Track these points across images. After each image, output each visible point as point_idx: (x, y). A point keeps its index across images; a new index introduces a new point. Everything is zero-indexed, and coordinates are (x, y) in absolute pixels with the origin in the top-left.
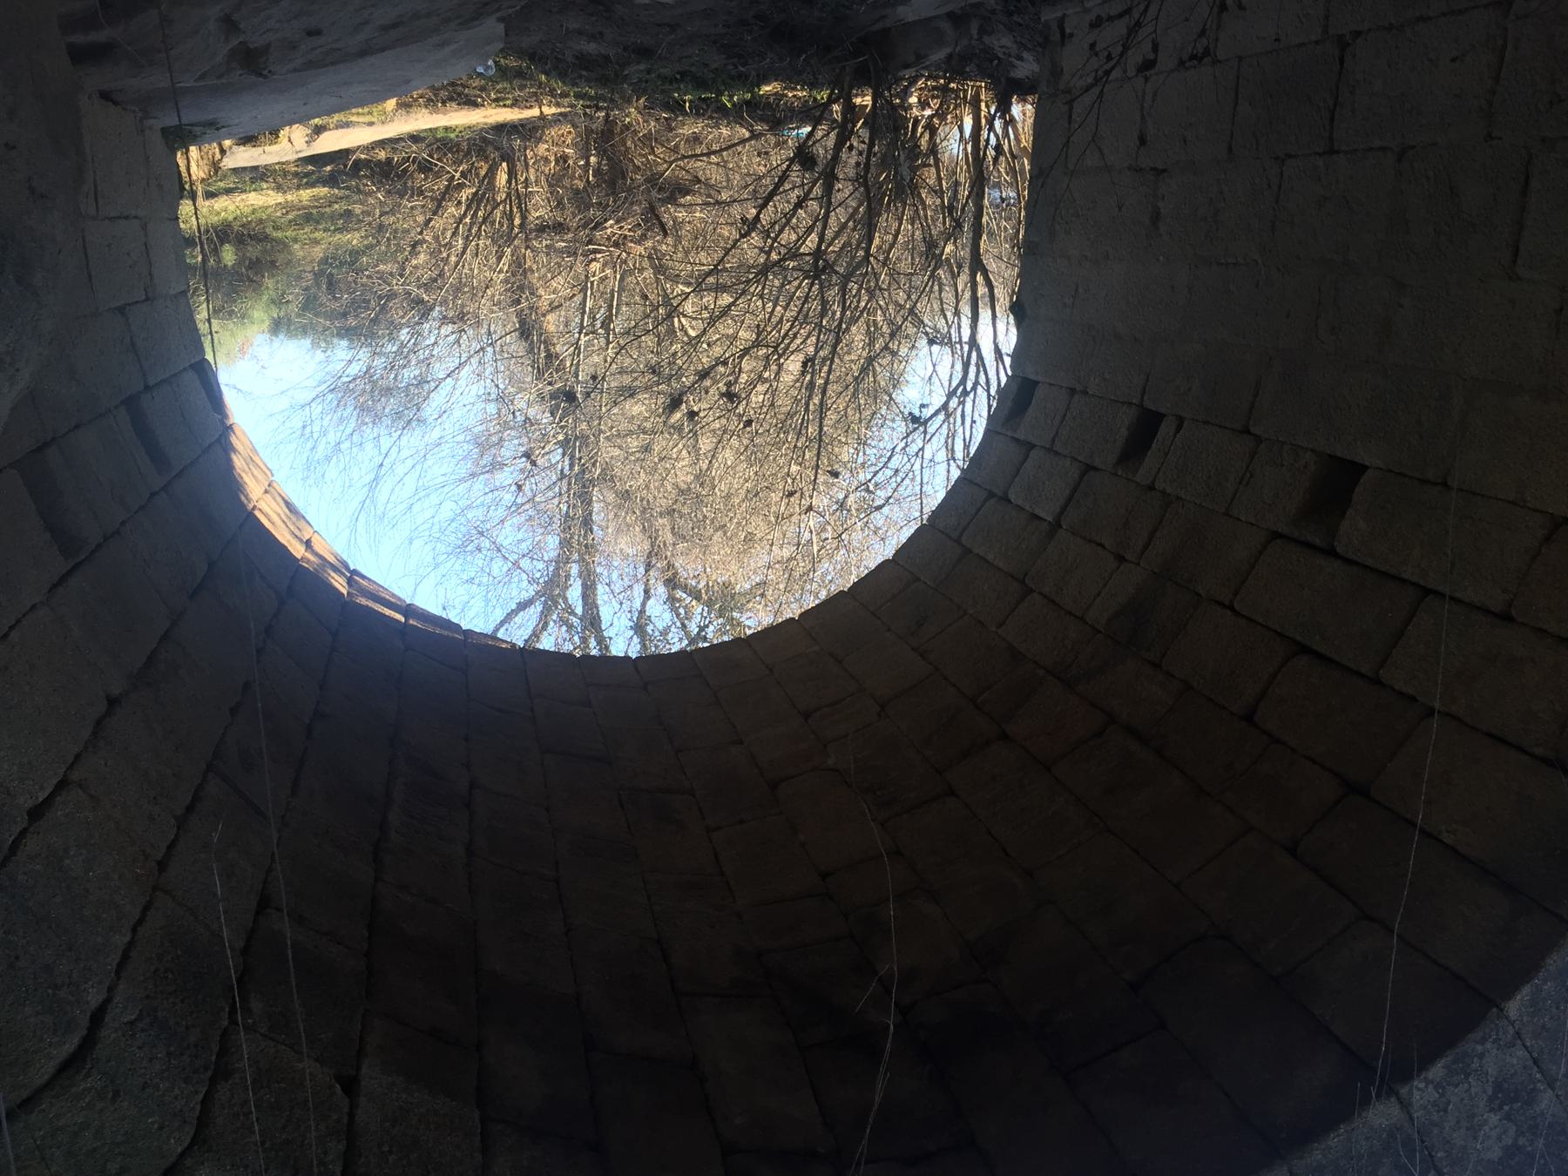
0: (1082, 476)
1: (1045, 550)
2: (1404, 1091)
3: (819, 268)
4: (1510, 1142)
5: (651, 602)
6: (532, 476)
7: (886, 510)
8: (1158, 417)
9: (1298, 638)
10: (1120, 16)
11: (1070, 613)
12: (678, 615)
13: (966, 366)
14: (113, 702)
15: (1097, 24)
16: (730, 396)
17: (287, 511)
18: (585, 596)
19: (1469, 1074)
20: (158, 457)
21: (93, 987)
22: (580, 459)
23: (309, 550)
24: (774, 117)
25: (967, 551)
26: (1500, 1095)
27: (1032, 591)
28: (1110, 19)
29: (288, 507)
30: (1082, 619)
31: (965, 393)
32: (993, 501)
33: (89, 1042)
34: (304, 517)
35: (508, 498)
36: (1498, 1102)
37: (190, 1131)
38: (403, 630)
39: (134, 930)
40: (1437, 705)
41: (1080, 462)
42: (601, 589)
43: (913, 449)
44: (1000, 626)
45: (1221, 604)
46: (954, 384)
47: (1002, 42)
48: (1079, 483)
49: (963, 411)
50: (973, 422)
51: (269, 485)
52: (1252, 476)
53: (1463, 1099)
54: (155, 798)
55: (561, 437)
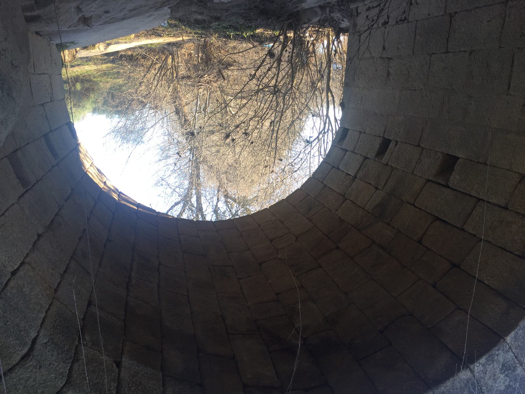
0: (364, 160)
2: (472, 367)
3: (276, 91)
4: (507, 384)
5: (219, 203)
6: (180, 160)
7: (298, 172)
8: (390, 141)
9: (436, 215)
10: (376, 6)
13: (325, 124)
15: (369, 9)
17: (98, 172)
20: (55, 154)
21: (32, 331)
22: (196, 155)
23: (105, 185)
24: (261, 40)
25: (325, 186)
26: (504, 368)
28: (373, 7)
29: (98, 171)
30: (364, 209)
31: (325, 133)
32: (334, 169)
33: (31, 350)
34: (104, 174)
35: (172, 168)
36: (503, 371)
39: (46, 312)
40: (483, 237)
41: (363, 156)
42: (203, 198)
43: (307, 152)
45: (410, 204)
46: (321, 130)
47: (337, 15)
50: (327, 142)
51: (92, 164)
52: (421, 161)
53: (492, 370)
54: (53, 268)
55: (189, 148)
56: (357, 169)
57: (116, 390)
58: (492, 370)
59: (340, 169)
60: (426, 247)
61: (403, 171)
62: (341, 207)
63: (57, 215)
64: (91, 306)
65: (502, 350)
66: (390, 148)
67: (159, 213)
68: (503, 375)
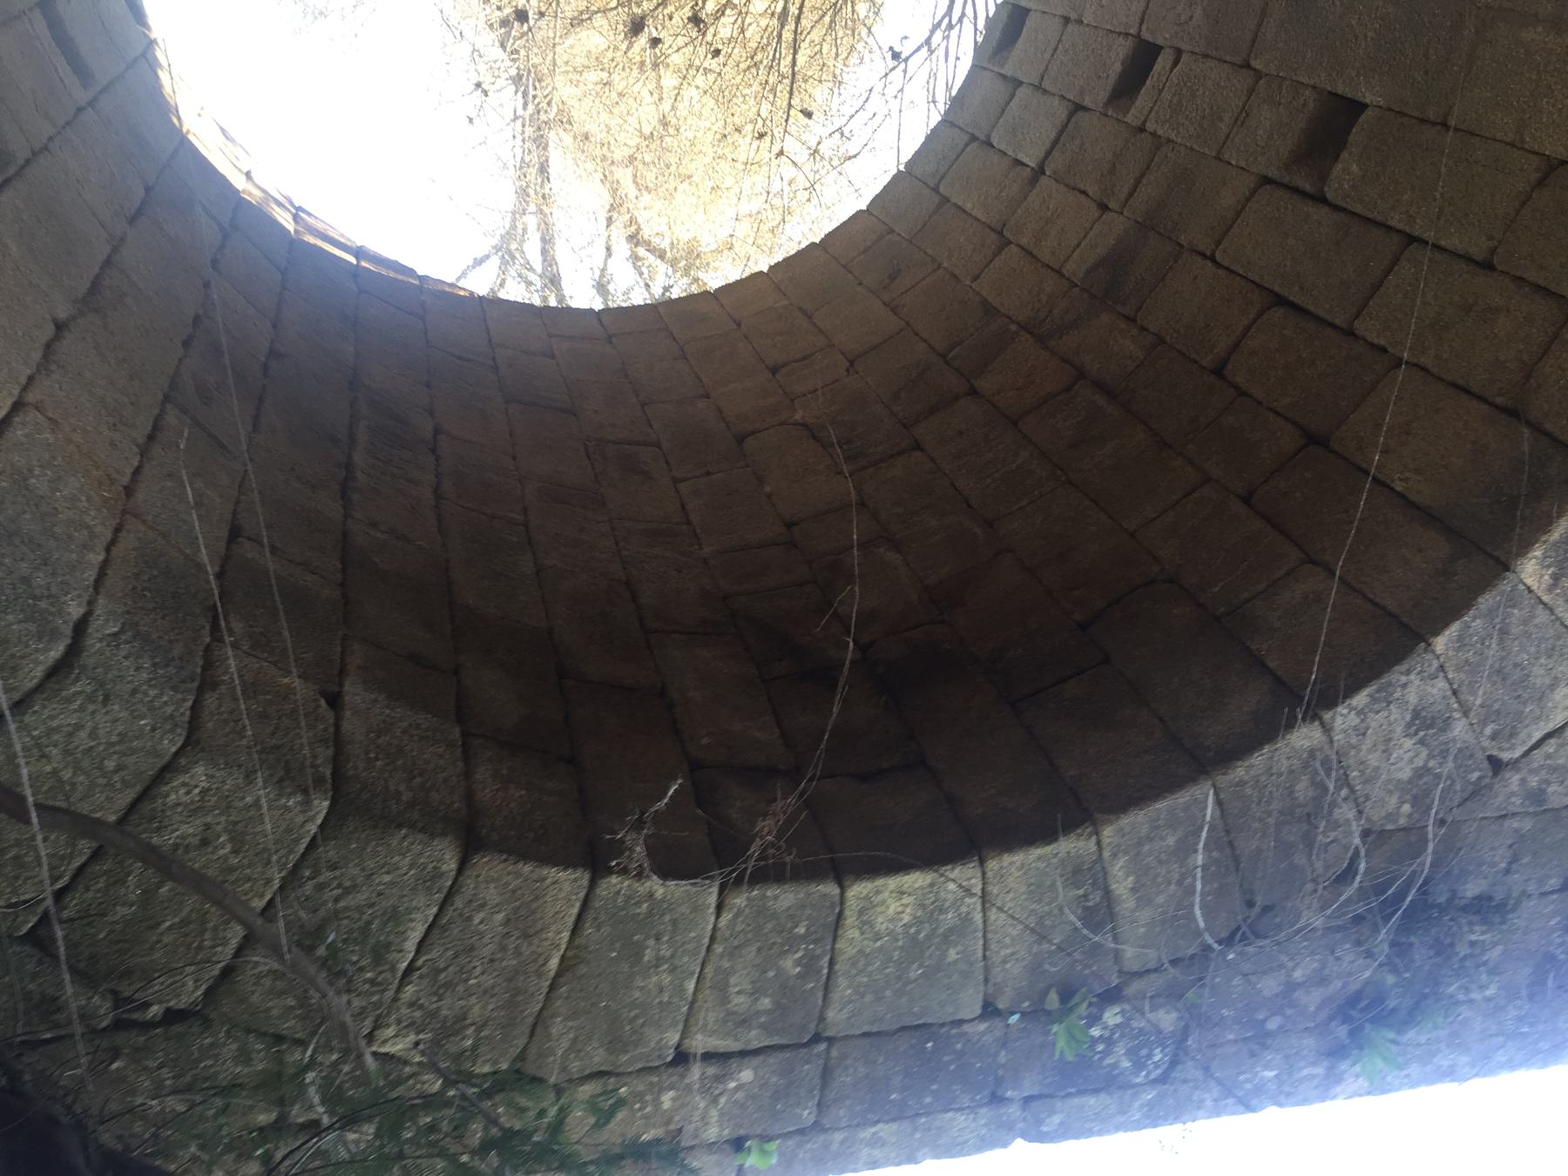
0: (1071, 115)
1: (1026, 198)
4: (1421, 763)
9: (1277, 289)
11: (1048, 266)
12: (641, 274)
14: (60, 327)
16: (695, 20)
18: (544, 252)
19: (1391, 702)
21: (72, 600)
22: (534, 97)
23: (250, 182)
26: (1417, 722)
27: (1010, 243)
30: (1058, 272)
31: (950, 27)
32: (975, 145)
33: (74, 650)
37: (181, 733)
38: (356, 272)
39: (108, 549)
41: (1069, 100)
43: (891, 91)
44: (975, 278)
48: (1067, 124)
49: (947, 48)
50: (958, 58)
52: (1247, 115)
54: (114, 425)
55: (513, 72)
56: (1048, 145)
57: (331, 766)
58: (1384, 727)
59: (993, 147)
60: (1236, 387)
61: (1192, 149)
62: (991, 266)
63: (108, 263)
64: (241, 539)
65: (1418, 674)
66: (1156, 75)
67: (424, 279)
68: (1413, 742)
